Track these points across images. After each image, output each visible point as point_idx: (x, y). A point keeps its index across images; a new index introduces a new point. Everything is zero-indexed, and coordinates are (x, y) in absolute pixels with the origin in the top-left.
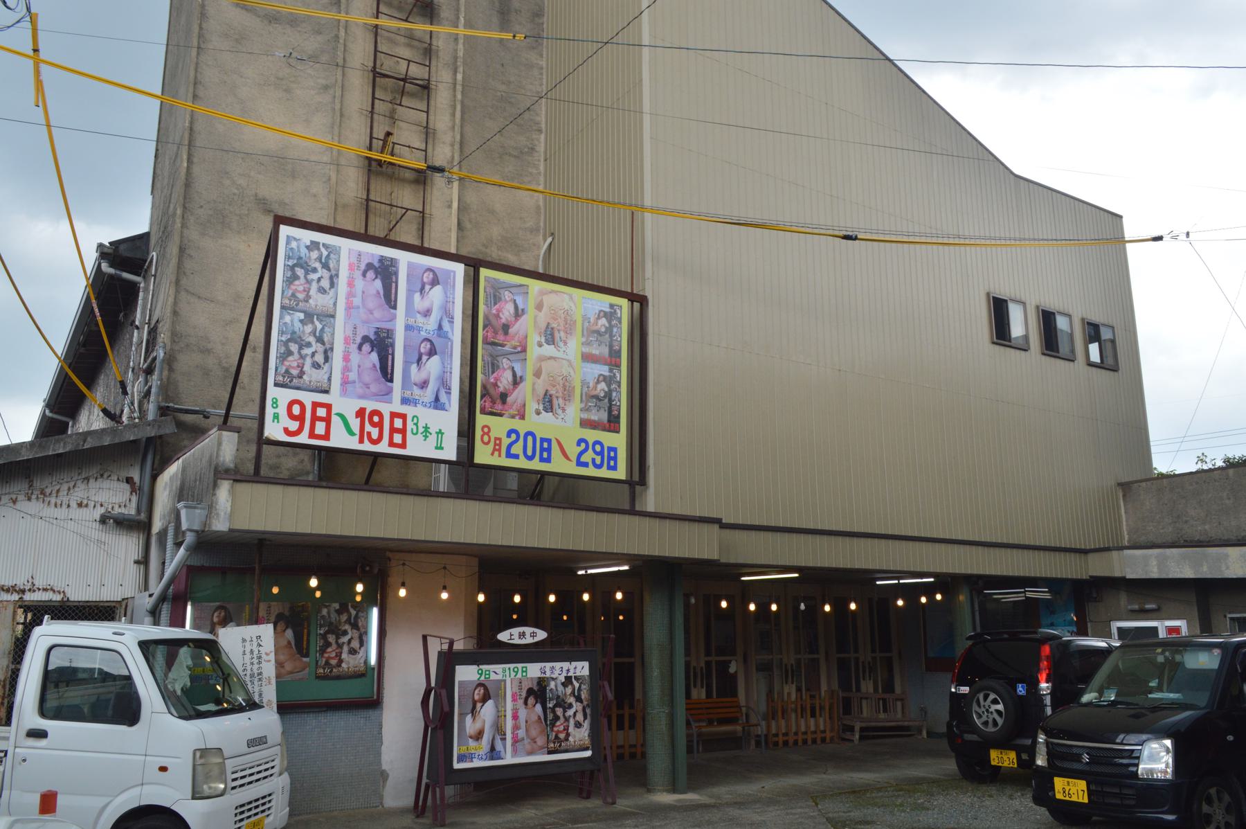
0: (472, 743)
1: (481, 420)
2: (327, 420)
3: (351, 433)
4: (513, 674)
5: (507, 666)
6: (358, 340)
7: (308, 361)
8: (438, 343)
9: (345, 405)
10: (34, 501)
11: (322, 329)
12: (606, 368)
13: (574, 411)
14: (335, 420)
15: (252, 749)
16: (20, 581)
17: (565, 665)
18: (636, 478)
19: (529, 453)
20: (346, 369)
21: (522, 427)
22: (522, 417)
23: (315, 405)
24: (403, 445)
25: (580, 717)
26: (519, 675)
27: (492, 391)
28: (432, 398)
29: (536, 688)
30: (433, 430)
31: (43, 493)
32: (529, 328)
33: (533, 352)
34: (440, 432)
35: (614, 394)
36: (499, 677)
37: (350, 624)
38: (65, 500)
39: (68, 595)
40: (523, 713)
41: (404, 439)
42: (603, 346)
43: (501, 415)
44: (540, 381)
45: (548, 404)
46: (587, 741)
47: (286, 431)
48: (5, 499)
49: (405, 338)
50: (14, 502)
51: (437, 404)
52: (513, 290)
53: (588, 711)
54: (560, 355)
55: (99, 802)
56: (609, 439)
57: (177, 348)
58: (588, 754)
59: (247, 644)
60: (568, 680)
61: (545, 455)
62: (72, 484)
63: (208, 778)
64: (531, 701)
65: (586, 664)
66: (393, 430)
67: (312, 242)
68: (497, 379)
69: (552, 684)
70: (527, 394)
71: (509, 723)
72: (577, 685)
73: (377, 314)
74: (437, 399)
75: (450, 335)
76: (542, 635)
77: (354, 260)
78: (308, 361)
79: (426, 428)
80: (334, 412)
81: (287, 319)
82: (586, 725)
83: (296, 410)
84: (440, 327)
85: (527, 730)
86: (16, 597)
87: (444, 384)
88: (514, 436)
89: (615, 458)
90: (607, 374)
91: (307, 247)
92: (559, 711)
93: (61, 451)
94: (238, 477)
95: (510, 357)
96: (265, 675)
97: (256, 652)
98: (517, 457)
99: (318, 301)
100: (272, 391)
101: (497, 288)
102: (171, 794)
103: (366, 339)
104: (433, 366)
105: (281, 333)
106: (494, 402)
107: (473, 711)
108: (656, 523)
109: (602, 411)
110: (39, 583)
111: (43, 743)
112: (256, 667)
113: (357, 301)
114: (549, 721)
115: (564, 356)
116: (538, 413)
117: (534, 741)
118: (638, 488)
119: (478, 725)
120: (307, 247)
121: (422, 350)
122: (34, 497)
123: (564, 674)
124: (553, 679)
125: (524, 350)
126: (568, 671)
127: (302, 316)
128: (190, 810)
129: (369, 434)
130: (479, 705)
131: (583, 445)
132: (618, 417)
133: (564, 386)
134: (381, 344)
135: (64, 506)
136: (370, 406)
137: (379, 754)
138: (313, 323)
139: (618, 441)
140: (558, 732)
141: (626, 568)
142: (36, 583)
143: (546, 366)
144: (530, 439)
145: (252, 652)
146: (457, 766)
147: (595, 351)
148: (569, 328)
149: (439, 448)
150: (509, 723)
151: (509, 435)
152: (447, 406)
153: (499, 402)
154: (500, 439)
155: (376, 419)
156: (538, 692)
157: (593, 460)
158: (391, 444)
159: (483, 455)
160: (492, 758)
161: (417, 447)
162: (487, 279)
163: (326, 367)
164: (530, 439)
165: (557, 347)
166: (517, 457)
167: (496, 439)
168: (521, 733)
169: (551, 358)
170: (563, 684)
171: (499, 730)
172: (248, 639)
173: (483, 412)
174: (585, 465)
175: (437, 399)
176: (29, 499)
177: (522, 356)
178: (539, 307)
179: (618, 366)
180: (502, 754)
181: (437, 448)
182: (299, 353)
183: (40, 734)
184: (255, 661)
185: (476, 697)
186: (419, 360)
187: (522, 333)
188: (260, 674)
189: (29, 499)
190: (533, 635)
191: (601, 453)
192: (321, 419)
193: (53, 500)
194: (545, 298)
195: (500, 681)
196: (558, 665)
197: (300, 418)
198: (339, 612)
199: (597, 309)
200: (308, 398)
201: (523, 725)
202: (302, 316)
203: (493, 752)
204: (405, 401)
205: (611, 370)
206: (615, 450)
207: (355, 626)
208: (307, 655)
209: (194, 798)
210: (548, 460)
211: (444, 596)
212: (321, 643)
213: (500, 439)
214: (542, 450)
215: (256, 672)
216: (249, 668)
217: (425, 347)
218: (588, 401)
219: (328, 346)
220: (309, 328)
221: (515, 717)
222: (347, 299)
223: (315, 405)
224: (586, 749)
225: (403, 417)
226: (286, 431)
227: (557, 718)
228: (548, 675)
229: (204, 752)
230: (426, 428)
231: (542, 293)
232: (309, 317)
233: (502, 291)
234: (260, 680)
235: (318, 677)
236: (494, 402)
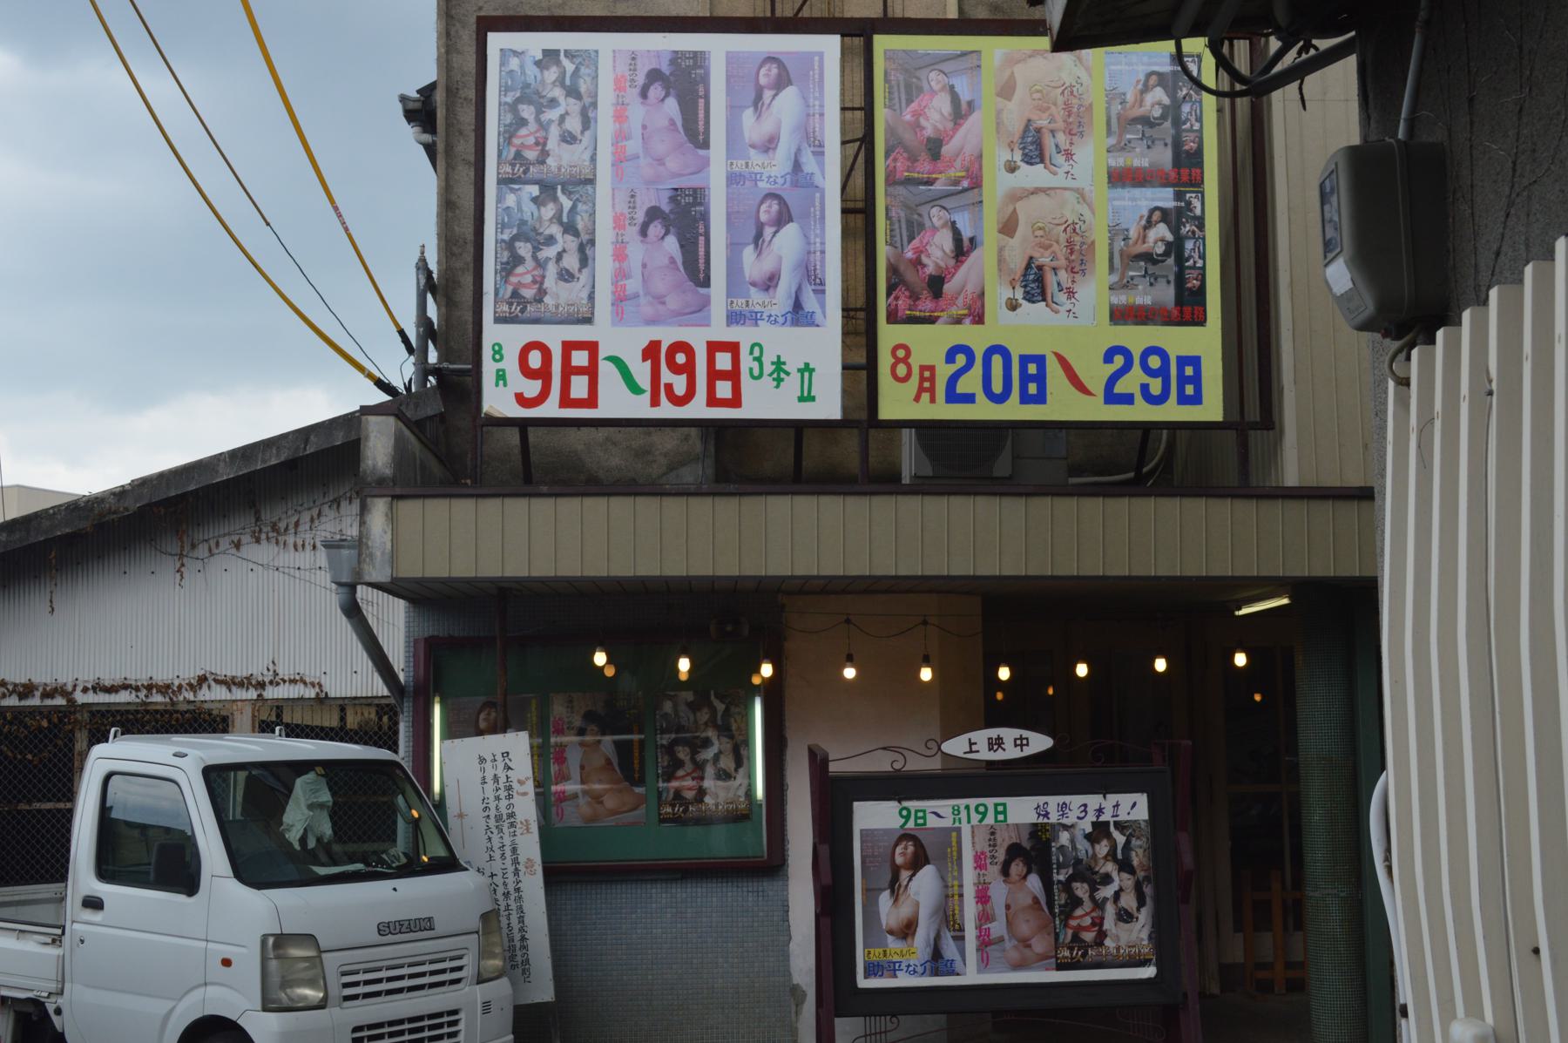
0: (893, 944)
1: (889, 335)
2: (591, 371)
3: (635, 389)
4: (975, 818)
5: (962, 802)
6: (640, 216)
7: (552, 270)
8: (793, 198)
9: (622, 341)
10: (264, 542)
11: (573, 209)
12: (1169, 192)
13: (1095, 292)
14: (606, 369)
15: (390, 938)
16: (258, 669)
17: (1094, 801)
18: (1253, 414)
19: (997, 387)
20: (620, 275)
21: (977, 338)
22: (979, 319)
23: (568, 347)
24: (735, 401)
25: (1128, 901)
26: (990, 820)
27: (910, 275)
28: (788, 305)
29: (1027, 845)
30: (792, 366)
31: (274, 528)
32: (987, 139)
33: (997, 184)
34: (807, 369)
35: (1189, 245)
36: (947, 823)
37: (716, 727)
38: (308, 537)
39: (326, 688)
40: (999, 892)
41: (736, 389)
42: (1159, 147)
43: (931, 320)
44: (1014, 242)
45: (1035, 284)
46: (1146, 948)
47: (521, 400)
48: (225, 543)
49: (729, 200)
50: (238, 546)
51: (798, 314)
52: (947, 67)
53: (1148, 890)
54: (1059, 181)
55: (161, 1007)
56: (1178, 340)
57: (458, 265)
58: (1149, 972)
59: (488, 765)
60: (1100, 830)
61: (1033, 388)
62: (315, 512)
63: (286, 984)
64: (1017, 868)
65: (1142, 799)
66: (714, 375)
67: (546, 52)
68: (919, 251)
69: (1064, 838)
70: (988, 271)
71: (970, 910)
72: (1120, 839)
73: (673, 164)
74: (798, 305)
75: (818, 180)
76: (1040, 742)
77: (623, 69)
78: (552, 270)
79: (779, 364)
80: (602, 354)
81: (511, 200)
82: (1144, 916)
83: (535, 360)
84: (797, 166)
85: (1009, 923)
86: (252, 694)
87: (811, 276)
88: (961, 360)
89: (1196, 380)
90: (1170, 204)
91: (538, 63)
92: (1081, 890)
93: (274, 462)
94: (398, 491)
95: (947, 203)
96: (520, 818)
97: (503, 780)
98: (969, 398)
99: (563, 159)
100: (492, 333)
101: (912, 67)
102: (236, 1000)
103: (653, 214)
104: (787, 243)
105: (501, 226)
106: (915, 297)
107: (894, 886)
108: (1299, 509)
109: (1162, 283)
110: (284, 671)
111: (97, 917)
112: (503, 803)
113: (633, 146)
114: (1058, 907)
115: (1070, 183)
116: (1013, 306)
117: (1025, 943)
118: (1255, 437)
119: (905, 911)
120: (538, 63)
121: (763, 217)
122: (263, 536)
123: (1091, 817)
124: (1066, 827)
125: (976, 184)
126: (1100, 811)
127: (535, 190)
128: (261, 1026)
129: (669, 387)
130: (905, 875)
131: (1119, 360)
132: (1201, 292)
133: (1070, 245)
134: (683, 216)
135: (308, 548)
136: (667, 335)
137: (786, 957)
138: (555, 199)
139: (1204, 342)
140: (1080, 928)
141: (1285, 601)
142: (280, 672)
143: (1025, 211)
144: (997, 360)
145: (496, 779)
146: (863, 983)
147: (1140, 160)
148: (1076, 125)
149: (806, 398)
150: (970, 910)
151: (950, 358)
152: (818, 317)
153: (927, 294)
154: (932, 368)
155: (681, 358)
156: (1034, 850)
157: (1145, 388)
158: (713, 401)
159: (897, 402)
160: (936, 973)
161: (763, 402)
162: (890, 55)
163: (584, 276)
164: (997, 360)
165: (1051, 166)
166: (969, 398)
167: (923, 368)
168: (997, 928)
169: (1035, 191)
170: (1088, 837)
171: (949, 919)
172: (489, 758)
173: (893, 318)
174: (1128, 399)
175: (798, 305)
176: (258, 541)
177: (971, 196)
178: (1006, 91)
179: (1197, 183)
180: (958, 966)
181: (801, 399)
182: (535, 258)
183: (94, 904)
184: (503, 794)
185: (899, 860)
186: (759, 236)
187: (969, 150)
188: (512, 815)
189: (258, 541)
190: (1021, 743)
191: (1163, 373)
192: (580, 371)
193: (291, 539)
194: (1019, 70)
195: (946, 832)
196: (1076, 801)
197: (544, 374)
198: (694, 707)
199: (1141, 71)
200: (553, 337)
201: (1000, 912)
202: (535, 190)
203: (937, 961)
204: (734, 318)
205: (1179, 196)
206: (1195, 361)
207: (725, 730)
208: (641, 782)
209: (265, 1009)
210: (1040, 398)
211: (850, 673)
212: (664, 761)
213: (932, 368)
214: (1025, 379)
215: (504, 812)
216: (492, 805)
217: (768, 211)
218: (1125, 267)
219: (585, 237)
220: (549, 211)
221: (983, 897)
222: (615, 144)
223: (568, 347)
224: (1143, 963)
225: (733, 348)
226: (521, 400)
227: (1076, 902)
228: (1054, 818)
229: (282, 940)
230: (779, 364)
231: (1011, 60)
232: (548, 190)
233: (922, 74)
234: (512, 825)
235: (663, 820)
236: (915, 297)
